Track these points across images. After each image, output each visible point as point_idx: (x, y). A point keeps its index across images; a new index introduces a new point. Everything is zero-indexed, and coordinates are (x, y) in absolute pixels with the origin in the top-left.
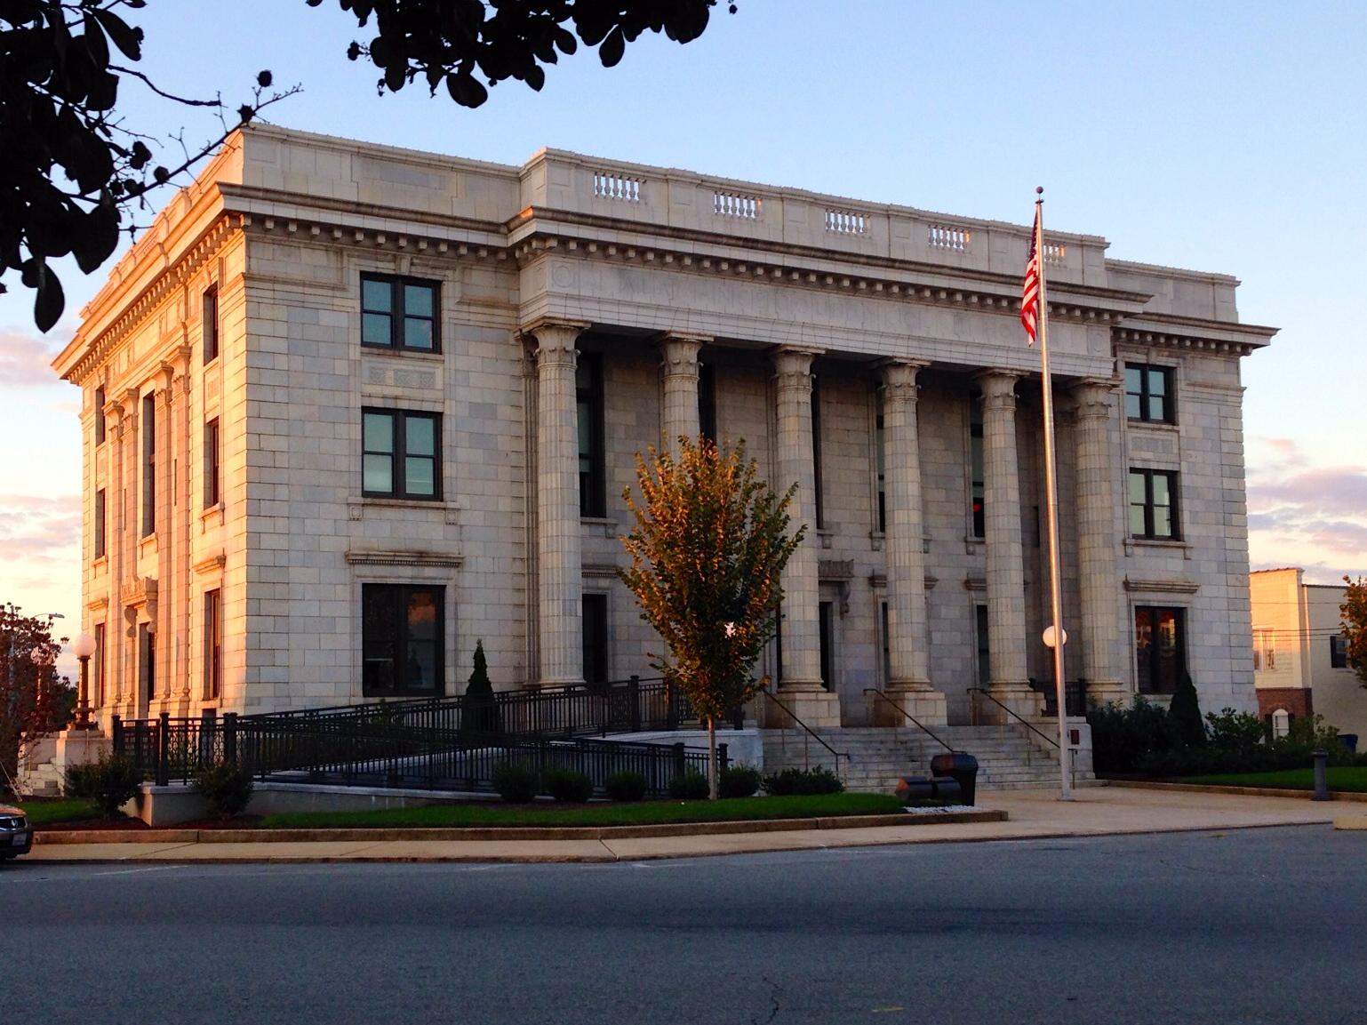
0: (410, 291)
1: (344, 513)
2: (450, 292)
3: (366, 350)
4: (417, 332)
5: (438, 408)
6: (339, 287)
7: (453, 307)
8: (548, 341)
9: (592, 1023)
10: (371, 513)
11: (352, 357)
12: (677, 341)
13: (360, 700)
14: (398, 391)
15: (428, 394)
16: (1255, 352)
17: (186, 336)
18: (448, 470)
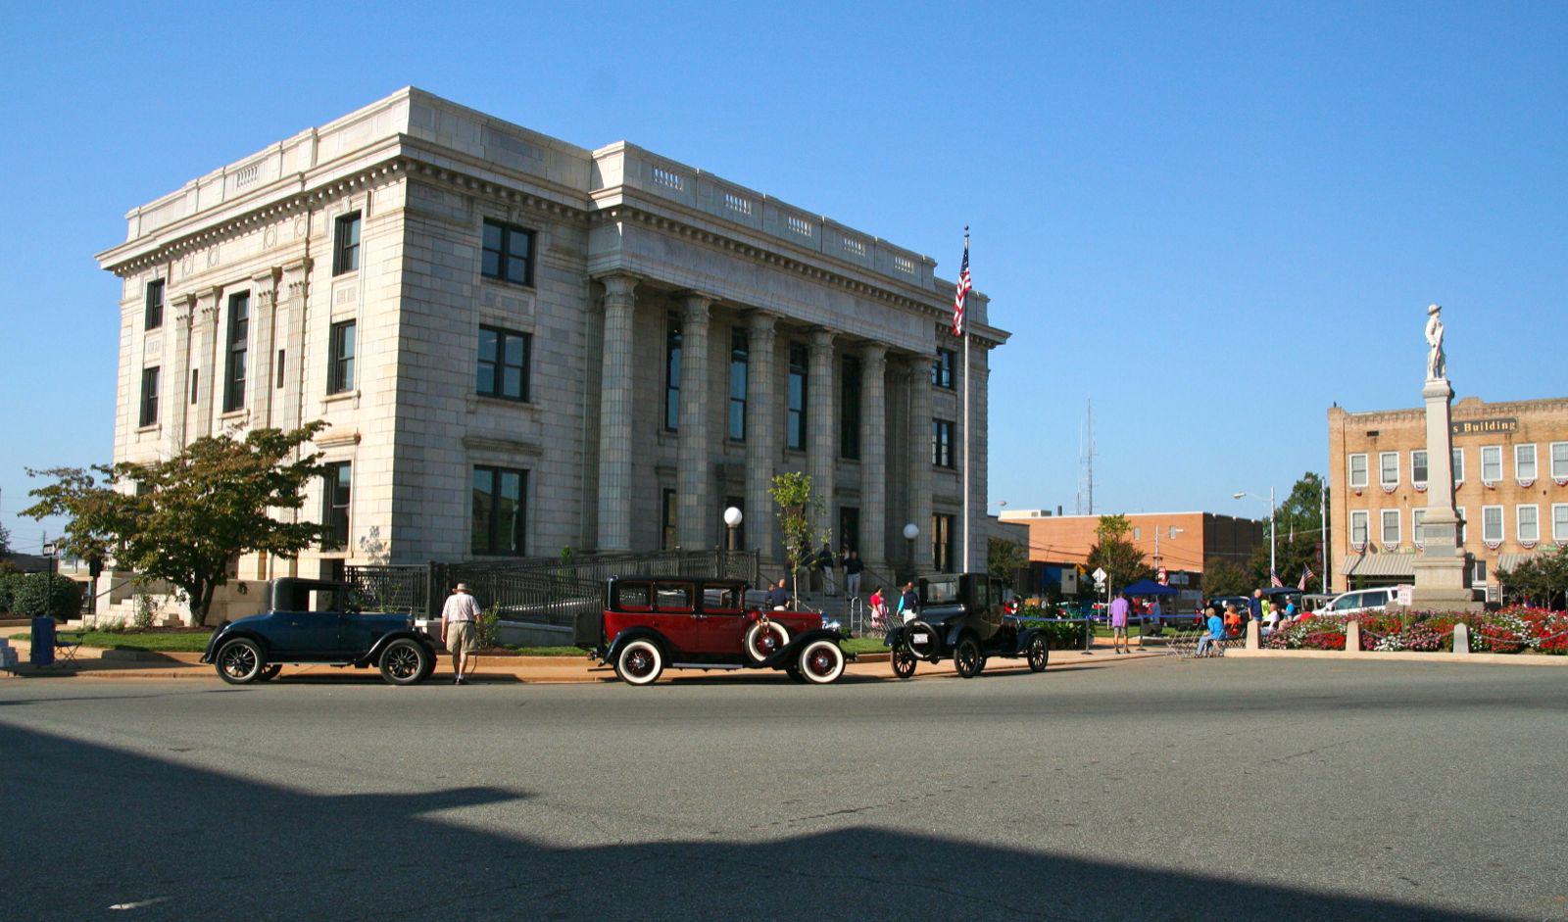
0: (513, 235)
1: (462, 406)
2: (543, 243)
3: (485, 278)
4: (516, 268)
5: (530, 330)
6: (469, 226)
7: (544, 252)
8: (615, 287)
9: (1566, 802)
10: (482, 409)
11: (474, 283)
12: (699, 296)
13: (469, 557)
14: (504, 314)
15: (524, 318)
16: (998, 347)
17: (307, 249)
18: (535, 379)
